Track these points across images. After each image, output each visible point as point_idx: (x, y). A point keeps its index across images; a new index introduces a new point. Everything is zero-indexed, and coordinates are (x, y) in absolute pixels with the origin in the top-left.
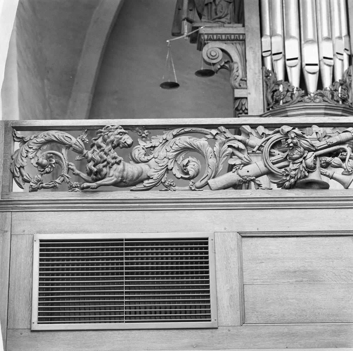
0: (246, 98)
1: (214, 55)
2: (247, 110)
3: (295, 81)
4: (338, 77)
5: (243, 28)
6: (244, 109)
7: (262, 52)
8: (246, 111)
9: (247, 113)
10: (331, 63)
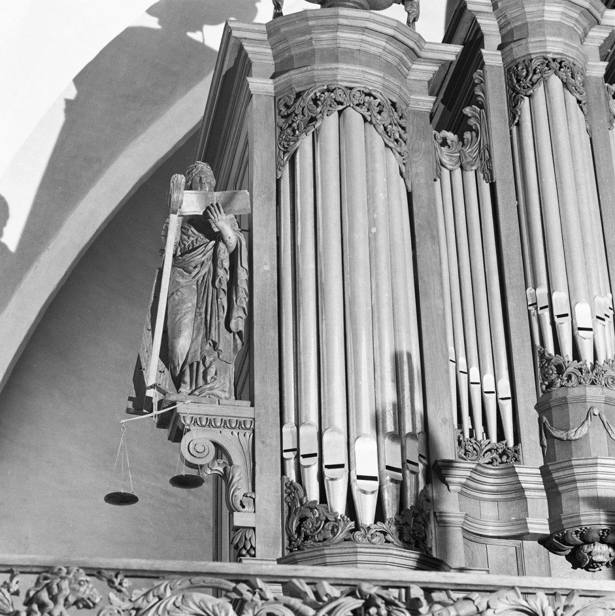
0: (254, 529)
1: (201, 451)
2: (254, 549)
3: (339, 505)
4: (410, 502)
5: (252, 408)
6: (248, 547)
7: (282, 451)
8: (253, 552)
9: (254, 556)
10: (397, 476)
